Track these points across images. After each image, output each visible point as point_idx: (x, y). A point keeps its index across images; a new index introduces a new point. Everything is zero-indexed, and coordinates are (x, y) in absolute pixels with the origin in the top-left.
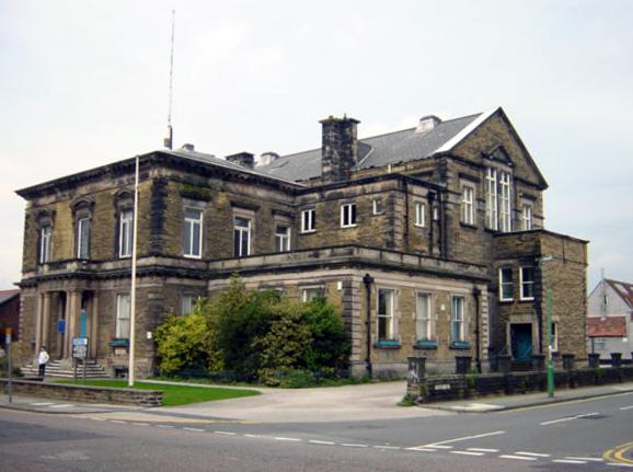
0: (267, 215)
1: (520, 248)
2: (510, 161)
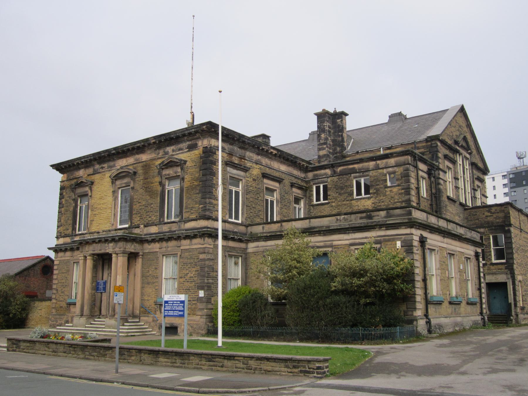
0: (287, 187)
1: (490, 219)
2: (470, 149)
